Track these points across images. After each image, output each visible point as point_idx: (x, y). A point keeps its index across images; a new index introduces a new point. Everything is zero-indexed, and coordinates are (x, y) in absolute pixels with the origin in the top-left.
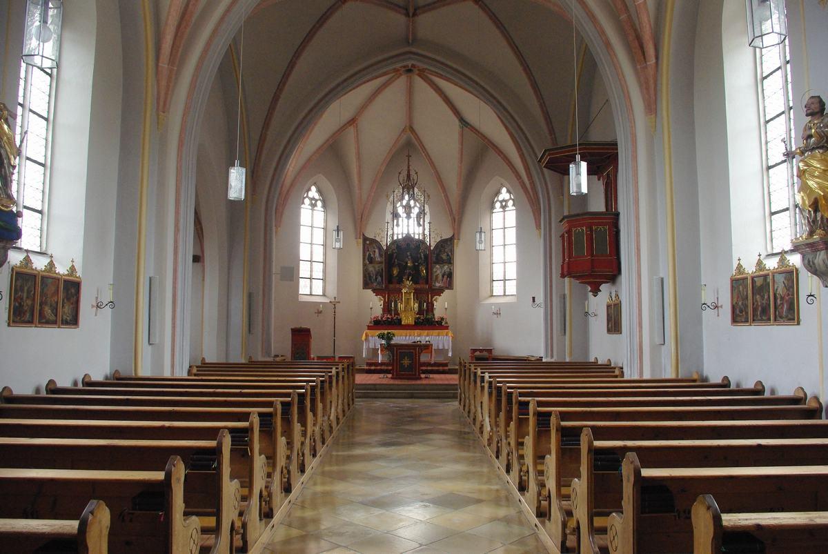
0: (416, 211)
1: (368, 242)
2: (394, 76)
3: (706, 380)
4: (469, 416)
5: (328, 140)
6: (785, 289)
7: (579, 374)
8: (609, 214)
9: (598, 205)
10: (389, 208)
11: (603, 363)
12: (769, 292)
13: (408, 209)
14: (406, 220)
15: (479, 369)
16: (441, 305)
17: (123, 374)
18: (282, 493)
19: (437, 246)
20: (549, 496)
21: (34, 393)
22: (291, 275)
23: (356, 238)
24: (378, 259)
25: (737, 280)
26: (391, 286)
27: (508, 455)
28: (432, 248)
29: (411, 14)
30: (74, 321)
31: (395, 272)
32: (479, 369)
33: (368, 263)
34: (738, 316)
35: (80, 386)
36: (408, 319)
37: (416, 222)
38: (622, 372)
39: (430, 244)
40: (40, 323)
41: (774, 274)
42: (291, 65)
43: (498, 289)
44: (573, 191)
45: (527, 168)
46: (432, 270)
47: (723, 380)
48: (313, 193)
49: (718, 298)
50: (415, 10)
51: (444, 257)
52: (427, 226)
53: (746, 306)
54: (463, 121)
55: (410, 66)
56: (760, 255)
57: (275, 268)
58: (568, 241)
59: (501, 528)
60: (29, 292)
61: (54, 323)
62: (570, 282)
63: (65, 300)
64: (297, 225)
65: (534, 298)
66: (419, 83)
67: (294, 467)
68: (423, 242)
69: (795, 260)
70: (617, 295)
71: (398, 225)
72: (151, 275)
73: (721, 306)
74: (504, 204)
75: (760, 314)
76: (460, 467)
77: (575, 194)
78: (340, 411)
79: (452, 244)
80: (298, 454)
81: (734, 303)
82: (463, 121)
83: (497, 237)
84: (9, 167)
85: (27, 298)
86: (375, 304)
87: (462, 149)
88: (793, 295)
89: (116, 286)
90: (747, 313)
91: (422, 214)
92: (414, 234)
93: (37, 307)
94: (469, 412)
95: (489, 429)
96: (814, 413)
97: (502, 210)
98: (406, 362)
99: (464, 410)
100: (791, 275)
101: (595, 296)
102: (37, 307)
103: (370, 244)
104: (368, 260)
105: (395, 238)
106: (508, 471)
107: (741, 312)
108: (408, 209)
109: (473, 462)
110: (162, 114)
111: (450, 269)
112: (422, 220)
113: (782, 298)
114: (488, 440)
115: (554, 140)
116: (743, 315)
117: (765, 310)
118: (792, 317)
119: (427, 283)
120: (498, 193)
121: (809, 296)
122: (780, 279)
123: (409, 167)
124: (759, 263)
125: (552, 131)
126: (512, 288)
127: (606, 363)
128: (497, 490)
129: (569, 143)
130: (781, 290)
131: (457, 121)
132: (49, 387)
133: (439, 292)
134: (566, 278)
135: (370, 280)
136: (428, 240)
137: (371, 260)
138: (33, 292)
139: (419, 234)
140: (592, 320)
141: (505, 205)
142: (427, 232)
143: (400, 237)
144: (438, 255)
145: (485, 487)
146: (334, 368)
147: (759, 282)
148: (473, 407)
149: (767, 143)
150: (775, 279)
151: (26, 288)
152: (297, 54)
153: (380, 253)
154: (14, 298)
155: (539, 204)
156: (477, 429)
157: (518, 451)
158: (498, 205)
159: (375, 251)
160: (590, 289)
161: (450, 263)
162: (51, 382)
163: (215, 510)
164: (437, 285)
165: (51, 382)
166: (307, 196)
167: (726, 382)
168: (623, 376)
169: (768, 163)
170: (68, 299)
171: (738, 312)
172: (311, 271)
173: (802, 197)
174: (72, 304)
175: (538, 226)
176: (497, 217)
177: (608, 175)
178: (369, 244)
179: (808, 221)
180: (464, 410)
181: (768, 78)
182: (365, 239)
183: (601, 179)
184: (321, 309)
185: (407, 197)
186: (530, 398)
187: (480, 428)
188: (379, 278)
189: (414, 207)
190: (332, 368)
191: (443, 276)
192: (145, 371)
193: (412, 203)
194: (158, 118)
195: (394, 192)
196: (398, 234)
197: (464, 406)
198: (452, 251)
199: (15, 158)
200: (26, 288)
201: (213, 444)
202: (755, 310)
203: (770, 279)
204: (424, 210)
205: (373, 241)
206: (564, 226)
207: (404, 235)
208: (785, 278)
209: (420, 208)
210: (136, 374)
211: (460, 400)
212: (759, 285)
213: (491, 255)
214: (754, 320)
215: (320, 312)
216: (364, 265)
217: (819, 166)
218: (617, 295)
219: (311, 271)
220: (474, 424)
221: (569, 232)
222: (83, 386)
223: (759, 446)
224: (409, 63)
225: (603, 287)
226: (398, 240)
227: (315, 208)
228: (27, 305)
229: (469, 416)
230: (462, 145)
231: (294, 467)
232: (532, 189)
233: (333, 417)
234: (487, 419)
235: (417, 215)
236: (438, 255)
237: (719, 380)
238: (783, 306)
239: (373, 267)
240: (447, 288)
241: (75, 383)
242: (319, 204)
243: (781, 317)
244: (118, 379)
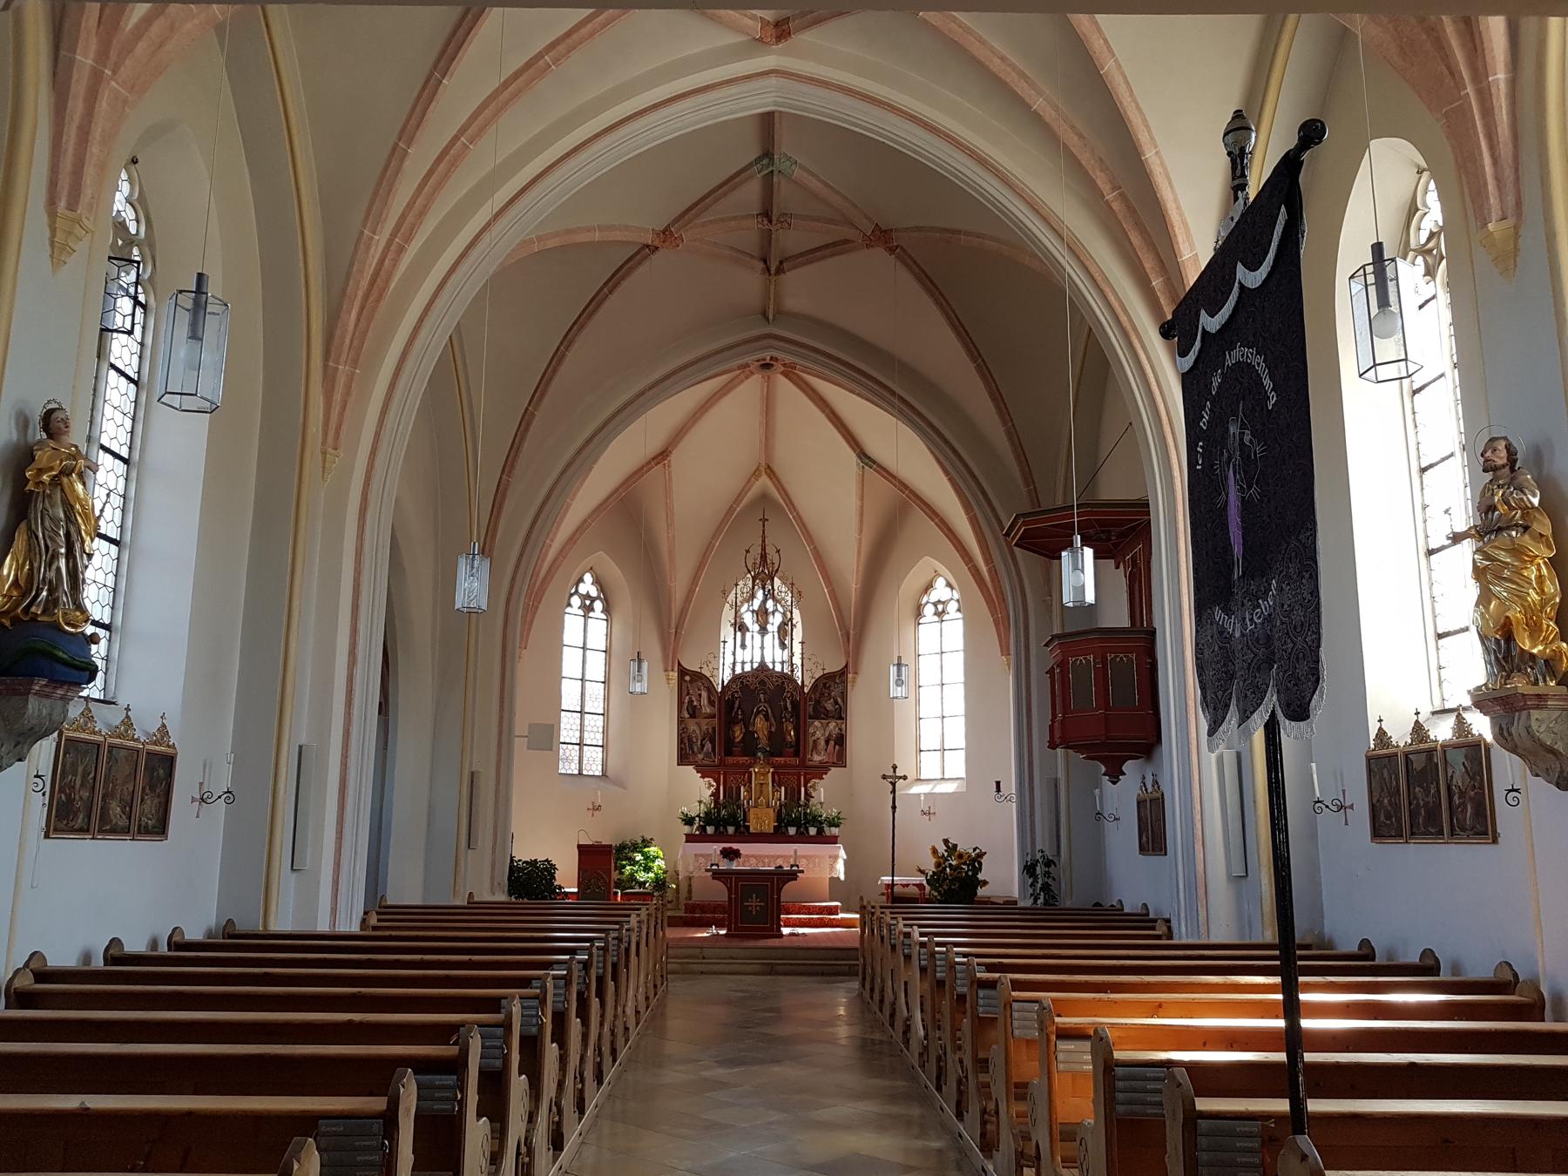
0: (776, 620)
1: (687, 678)
2: (740, 374)
3: (1330, 945)
4: (881, 1011)
5: (616, 490)
7: (473, 917)
8: (1139, 632)
9: (1117, 616)
10: (728, 615)
11: (1135, 911)
12: (1438, 783)
13: (762, 615)
14: (781, 651)
15: (900, 920)
16: (824, 794)
17: (241, 927)
18: (549, 1149)
19: (815, 686)
20: (1038, 1157)
21: (81, 964)
22: (546, 738)
23: (666, 670)
24: (707, 710)
25: (1379, 758)
26: (730, 760)
27: (959, 1082)
28: (806, 690)
29: (773, 270)
30: (160, 829)
31: (738, 733)
32: (900, 920)
33: (687, 716)
34: (1385, 826)
36: (760, 819)
37: (777, 642)
38: (1169, 928)
39: (803, 682)
40: (101, 831)
41: (1445, 746)
42: (558, 358)
43: (929, 766)
44: (1068, 599)
45: (988, 559)
46: (806, 732)
47: (1360, 947)
48: (588, 586)
49: (1344, 791)
50: (781, 263)
51: (829, 706)
52: (797, 649)
53: (1397, 807)
54: (863, 455)
55: (768, 358)
56: (1417, 713)
57: (521, 727)
58: (1060, 678)
60: (85, 774)
61: (125, 831)
62: (1067, 755)
63: (147, 791)
64: (557, 645)
65: (998, 784)
66: (784, 386)
67: (568, 1103)
68: (787, 679)
69: (1481, 725)
70: (1156, 782)
71: (743, 646)
72: (303, 742)
73: (1351, 807)
74: (940, 607)
76: (869, 1107)
77: (1071, 605)
78: (641, 998)
79: (844, 682)
80: (575, 1078)
81: (1375, 801)
82: (863, 455)
83: (928, 670)
84: (82, 557)
85: (82, 785)
86: (697, 791)
87: (862, 507)
88: (1482, 787)
89: (240, 767)
90: (1399, 820)
91: (784, 630)
92: (774, 663)
93: (98, 799)
94: (882, 1001)
95: (922, 1033)
96: (1533, 1010)
97: (936, 618)
98: (754, 903)
99: (872, 998)
100: (1473, 749)
101: (1114, 783)
102: (98, 799)
103: (691, 681)
104: (688, 710)
105: (738, 670)
106: (960, 1116)
107: (1388, 817)
108: (762, 615)
109: (893, 1098)
110: (332, 451)
111: (840, 729)
112: (788, 638)
113: (1462, 794)
114: (921, 1055)
115: (1034, 495)
116: (1392, 823)
117: (1433, 816)
118: (1483, 829)
119: (796, 754)
120: (929, 587)
121: (1510, 791)
122: (1458, 759)
123: (764, 541)
124: (1418, 730)
125: (1028, 477)
126: (957, 765)
128: (939, 1151)
129: (1059, 503)
130: (1459, 779)
131: (852, 457)
132: (111, 952)
133: (821, 771)
134: (1058, 750)
135: (691, 748)
136: (799, 674)
137: (694, 712)
138: (92, 775)
139: (782, 663)
140: (1109, 826)
141: (943, 611)
142: (797, 660)
143: (748, 668)
144: (818, 702)
145: (919, 1143)
146: (633, 916)
147: (1419, 763)
148: (889, 990)
149: (1425, 507)
150: (1448, 758)
151: (80, 769)
152: (568, 340)
153: (709, 698)
154: (60, 789)
155: (1006, 608)
156: (898, 1036)
157: (977, 1077)
158: (929, 610)
159: (700, 695)
160: (1103, 769)
161: (841, 718)
162: (115, 942)
164: (817, 758)
165: (115, 942)
166: (576, 591)
167: (1365, 951)
168: (1170, 937)
169: (1427, 543)
170: (152, 789)
171: (1382, 818)
172: (582, 731)
173: (1482, 613)
174: (158, 796)
175: (1005, 650)
176: (928, 632)
177: (1134, 559)
178: (690, 681)
179: (1497, 658)
180: (872, 998)
181: (1422, 392)
182: (683, 672)
183: (1122, 566)
184: (599, 802)
185: (760, 594)
186: (997, 975)
187: (905, 1033)
188: (708, 746)
189: (773, 613)
190: (629, 916)
191: (827, 742)
192: (283, 921)
193: (770, 604)
194: (324, 460)
195: (737, 585)
196: (743, 663)
197: (872, 990)
198: (844, 695)
199: (92, 540)
200: (80, 769)
201: (450, 1051)
202: (1413, 815)
203: (1438, 758)
204: (791, 619)
205: (698, 677)
206: (1051, 658)
207: (755, 665)
208: (1466, 757)
209: (784, 614)
210: (265, 925)
211: (864, 979)
212: (1419, 769)
213: (918, 702)
214: (1412, 834)
215: (598, 808)
216: (681, 720)
217: (1508, 560)
218: (1156, 782)
219: (582, 731)
220: (892, 1025)
221: (1062, 664)
222: (169, 950)
223: (1413, 1065)
224: (767, 355)
225: (1128, 766)
226: (744, 676)
227: (591, 614)
228: (81, 798)
229: (881, 1011)
230: (862, 499)
231: (568, 1103)
232: (992, 581)
233: (630, 1011)
234: (918, 1016)
235: (779, 628)
236: (818, 702)
237: (1354, 948)
238: (1465, 809)
239: (698, 724)
240: (835, 765)
241: (154, 944)
242: (598, 605)
243: (1463, 829)
244: (231, 937)
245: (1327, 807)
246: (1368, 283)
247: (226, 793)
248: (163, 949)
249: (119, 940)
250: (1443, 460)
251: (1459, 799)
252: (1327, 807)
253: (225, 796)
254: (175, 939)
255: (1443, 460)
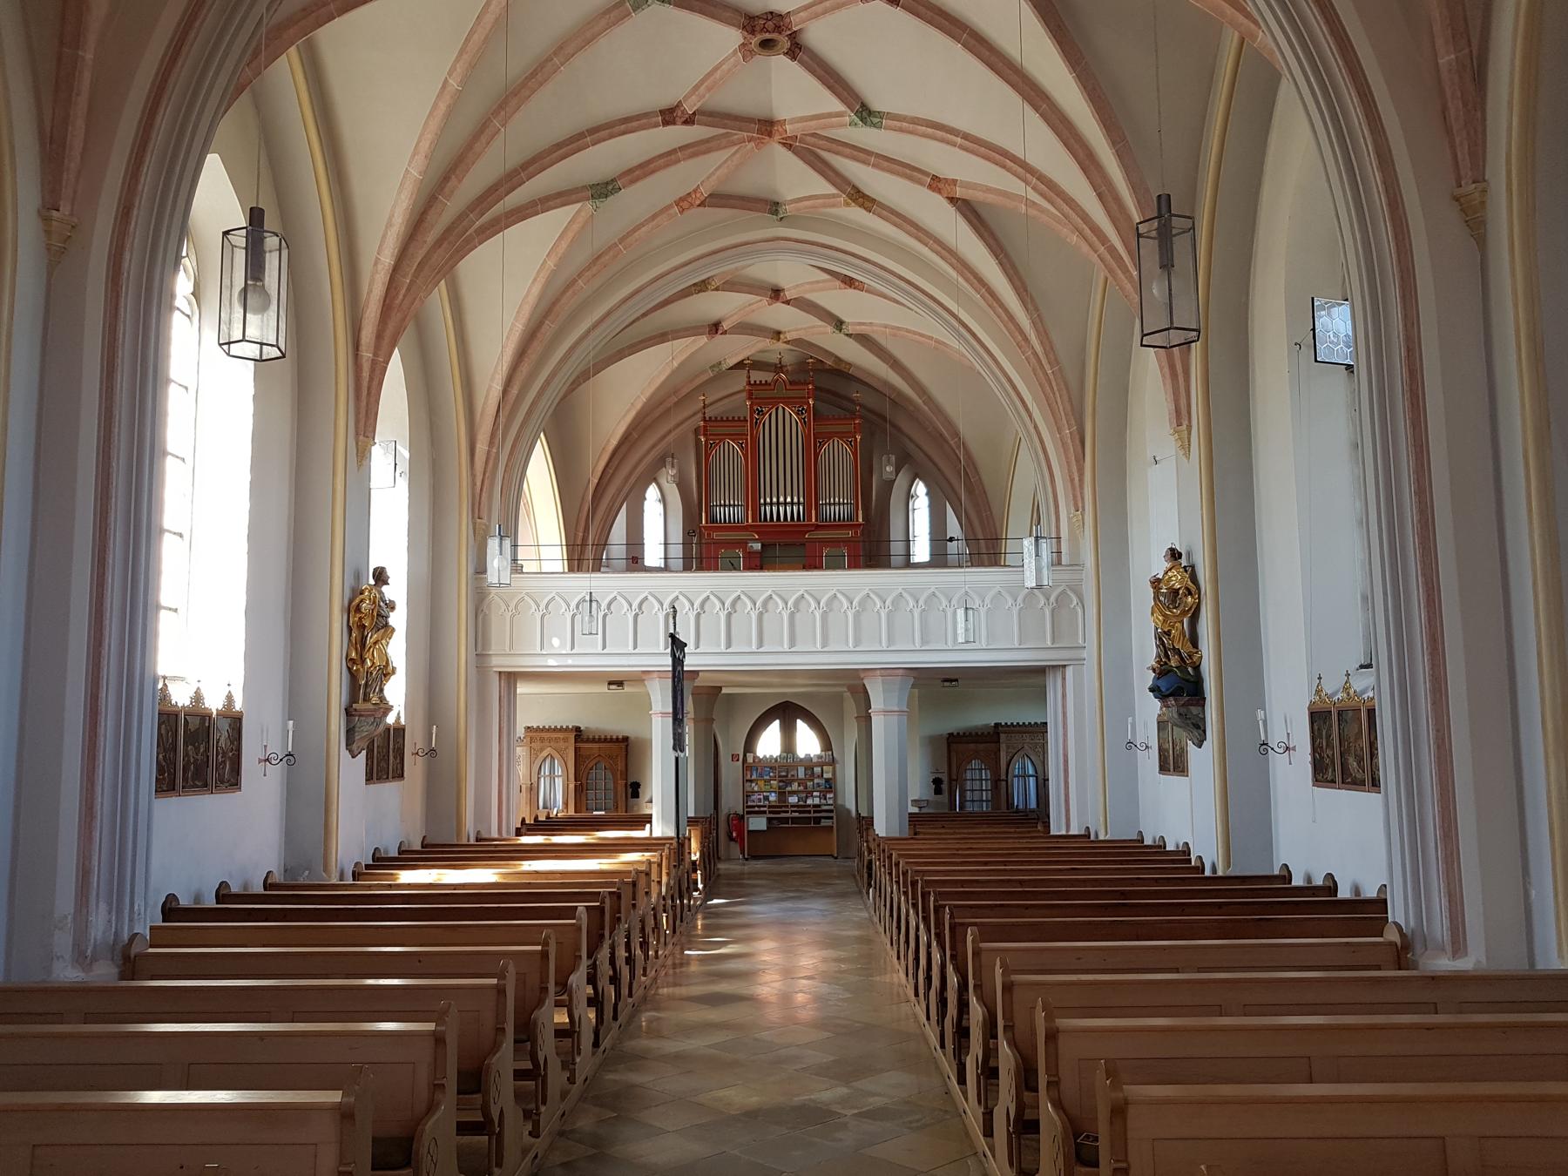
6: (228, 740)
35: (472, 841)
59: (1051, 672)
75: (192, 776)
116: (164, 779)
122: (224, 726)
127: (1083, 833)
147: (194, 724)
162: (223, 885)
163: (686, 952)
165: (171, 898)
243: (222, 782)
245: (1272, 749)
246: (264, 347)
247: (287, 755)
248: (472, 841)
249: (174, 895)
250: (177, 457)
251: (222, 757)
252: (1272, 749)
253: (286, 758)
254: (377, 855)
255: (177, 457)
